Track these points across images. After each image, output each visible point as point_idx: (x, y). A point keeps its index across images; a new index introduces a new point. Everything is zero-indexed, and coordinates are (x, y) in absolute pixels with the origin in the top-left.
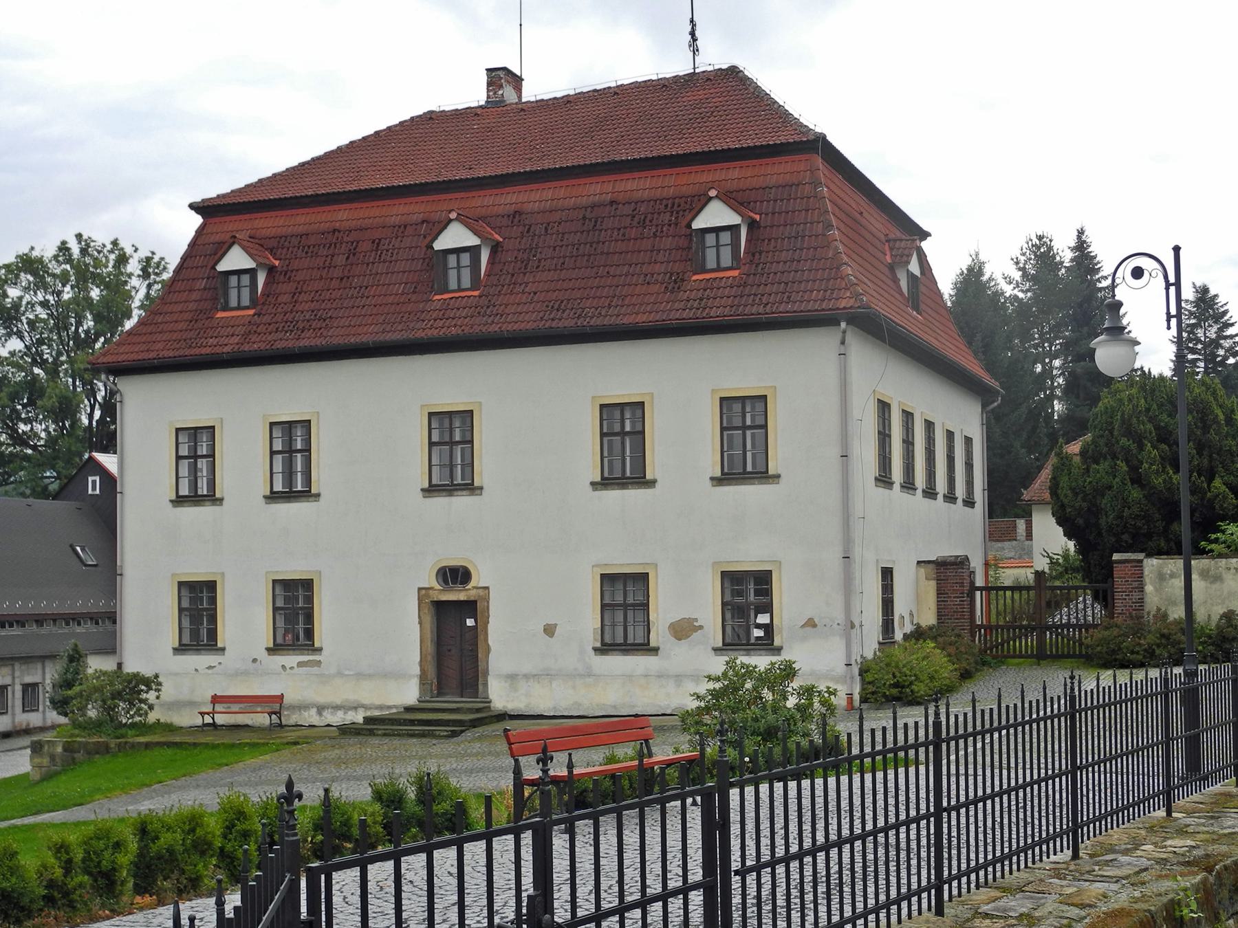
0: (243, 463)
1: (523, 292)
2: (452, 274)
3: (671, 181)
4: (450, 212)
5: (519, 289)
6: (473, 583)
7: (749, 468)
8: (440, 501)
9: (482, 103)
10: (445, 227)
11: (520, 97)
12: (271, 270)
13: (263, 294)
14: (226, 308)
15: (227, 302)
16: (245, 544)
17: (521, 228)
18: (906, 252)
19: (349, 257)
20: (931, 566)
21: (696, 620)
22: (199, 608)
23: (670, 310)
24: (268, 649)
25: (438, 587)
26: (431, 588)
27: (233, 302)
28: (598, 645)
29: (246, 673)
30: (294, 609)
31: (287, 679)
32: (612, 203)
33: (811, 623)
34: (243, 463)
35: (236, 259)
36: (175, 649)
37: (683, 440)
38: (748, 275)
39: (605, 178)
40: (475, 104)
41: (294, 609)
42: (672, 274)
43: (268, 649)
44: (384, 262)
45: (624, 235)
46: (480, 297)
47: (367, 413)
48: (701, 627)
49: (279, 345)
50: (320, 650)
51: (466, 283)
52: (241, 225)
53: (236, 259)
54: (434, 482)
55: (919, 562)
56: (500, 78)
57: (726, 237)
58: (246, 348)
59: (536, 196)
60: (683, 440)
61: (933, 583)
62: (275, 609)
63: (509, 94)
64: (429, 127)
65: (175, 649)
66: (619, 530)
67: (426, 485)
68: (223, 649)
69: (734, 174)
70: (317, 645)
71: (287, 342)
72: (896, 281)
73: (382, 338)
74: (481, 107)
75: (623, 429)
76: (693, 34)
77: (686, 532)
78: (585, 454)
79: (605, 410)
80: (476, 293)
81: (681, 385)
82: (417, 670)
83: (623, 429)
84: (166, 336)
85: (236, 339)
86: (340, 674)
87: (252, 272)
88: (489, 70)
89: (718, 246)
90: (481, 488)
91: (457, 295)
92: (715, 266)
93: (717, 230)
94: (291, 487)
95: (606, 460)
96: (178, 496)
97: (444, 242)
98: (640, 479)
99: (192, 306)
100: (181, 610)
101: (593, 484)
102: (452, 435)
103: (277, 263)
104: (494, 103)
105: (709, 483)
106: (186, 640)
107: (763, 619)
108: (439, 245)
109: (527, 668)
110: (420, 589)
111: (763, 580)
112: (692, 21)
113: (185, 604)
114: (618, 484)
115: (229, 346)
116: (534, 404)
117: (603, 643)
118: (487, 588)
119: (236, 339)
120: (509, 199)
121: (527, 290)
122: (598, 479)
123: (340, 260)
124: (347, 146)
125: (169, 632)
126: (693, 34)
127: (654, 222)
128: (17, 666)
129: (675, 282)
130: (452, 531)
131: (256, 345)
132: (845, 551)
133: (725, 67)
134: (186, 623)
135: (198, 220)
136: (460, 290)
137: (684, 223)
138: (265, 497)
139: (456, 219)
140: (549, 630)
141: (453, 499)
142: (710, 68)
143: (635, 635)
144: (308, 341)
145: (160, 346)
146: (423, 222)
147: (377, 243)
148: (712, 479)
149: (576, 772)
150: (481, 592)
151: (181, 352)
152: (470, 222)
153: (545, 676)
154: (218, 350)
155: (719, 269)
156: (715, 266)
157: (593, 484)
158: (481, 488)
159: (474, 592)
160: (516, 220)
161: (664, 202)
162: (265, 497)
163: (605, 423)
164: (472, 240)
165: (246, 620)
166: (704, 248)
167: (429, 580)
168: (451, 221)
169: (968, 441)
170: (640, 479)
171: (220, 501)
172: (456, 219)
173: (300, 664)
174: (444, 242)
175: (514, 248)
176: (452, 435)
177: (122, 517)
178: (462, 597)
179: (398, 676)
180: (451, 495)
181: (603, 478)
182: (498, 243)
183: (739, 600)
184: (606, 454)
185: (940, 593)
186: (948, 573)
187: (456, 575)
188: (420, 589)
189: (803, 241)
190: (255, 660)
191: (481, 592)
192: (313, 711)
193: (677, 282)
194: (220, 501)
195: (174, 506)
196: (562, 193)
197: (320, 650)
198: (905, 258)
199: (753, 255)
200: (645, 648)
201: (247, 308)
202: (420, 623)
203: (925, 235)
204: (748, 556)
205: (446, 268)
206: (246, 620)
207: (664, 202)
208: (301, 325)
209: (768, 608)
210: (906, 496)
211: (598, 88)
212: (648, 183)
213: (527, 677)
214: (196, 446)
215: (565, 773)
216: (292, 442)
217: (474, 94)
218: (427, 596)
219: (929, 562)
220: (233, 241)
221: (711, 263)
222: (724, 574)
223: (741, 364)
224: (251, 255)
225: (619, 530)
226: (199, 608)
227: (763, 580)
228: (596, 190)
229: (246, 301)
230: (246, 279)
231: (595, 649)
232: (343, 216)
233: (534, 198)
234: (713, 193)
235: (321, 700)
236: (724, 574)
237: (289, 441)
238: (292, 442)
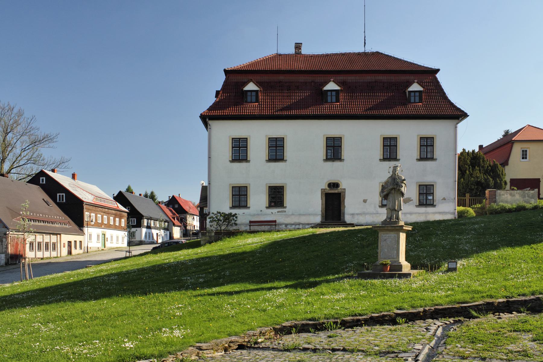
6: (340, 187)
24: (267, 207)
29: (258, 215)
30: (276, 196)
33: (444, 199)
37: (258, 149)
41: (276, 196)
50: (286, 207)
56: (298, 46)
69: (259, 78)
78: (378, 151)
82: (320, 213)
86: (293, 214)
89: (415, 96)
93: (415, 92)
97: (247, 88)
98: (245, 159)
105: (415, 161)
107: (430, 198)
109: (357, 212)
130: (332, 172)
140: (365, 201)
141: (334, 163)
143: (243, 204)
149: (108, 245)
152: (257, 83)
153: (364, 214)
166: (327, 96)
167: (325, 186)
170: (245, 159)
173: (278, 212)
174: (247, 88)
178: (336, 191)
179: (316, 215)
187: (334, 185)
188: (322, 189)
192: (284, 226)
194: (399, 160)
197: (286, 207)
200: (433, 205)
202: (322, 199)
204: (428, 180)
213: (358, 214)
215: (100, 245)
220: (251, 80)
231: (379, 206)
232: (282, 78)
235: (286, 222)
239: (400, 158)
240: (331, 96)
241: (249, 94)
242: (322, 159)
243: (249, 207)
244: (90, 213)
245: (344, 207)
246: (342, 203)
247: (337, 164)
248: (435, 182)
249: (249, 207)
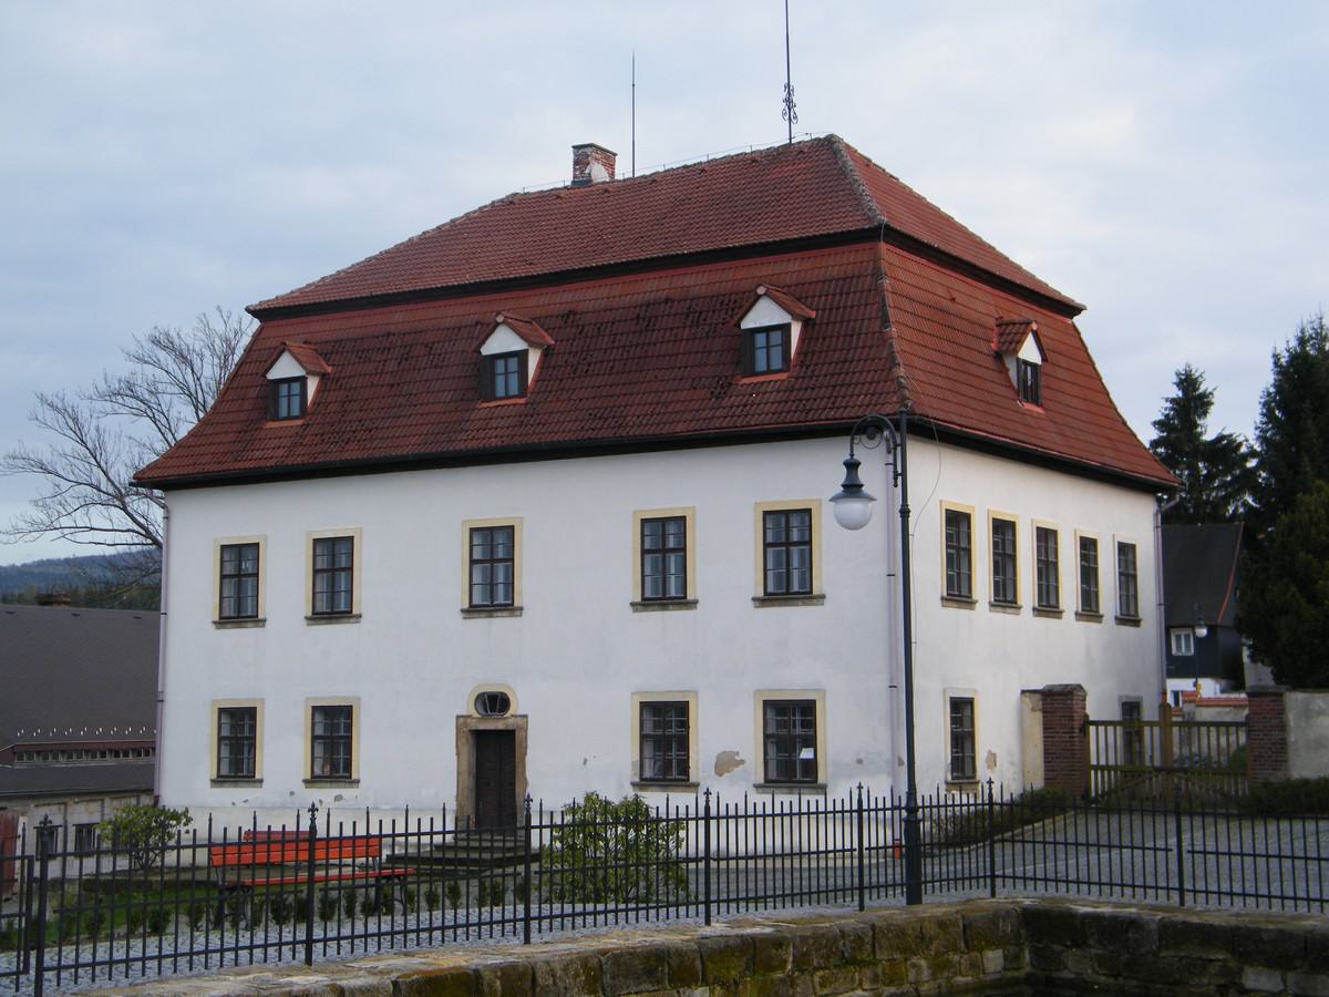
0: (286, 582)
1: (569, 400)
2: (500, 381)
3: (730, 275)
4: (498, 313)
5: (565, 395)
6: (511, 711)
7: (796, 588)
8: (480, 624)
9: (568, 183)
10: (492, 331)
11: (612, 175)
12: (323, 377)
13: (314, 403)
14: (276, 418)
15: (277, 412)
16: (285, 666)
17: (574, 330)
18: (1016, 338)
19: (377, 375)
20: (1038, 696)
21: (737, 754)
22: (238, 735)
23: (711, 419)
25: (476, 715)
26: (470, 716)
27: (283, 412)
28: (637, 780)
30: (333, 733)
31: (340, 811)
32: (667, 301)
34: (286, 582)
35: (286, 367)
36: (213, 781)
37: (726, 558)
38: (797, 378)
39: (663, 274)
40: (560, 185)
41: (333, 733)
42: (720, 378)
43: (305, 781)
44: (436, 367)
45: (676, 336)
46: (526, 404)
47: (410, 529)
48: (742, 762)
49: (321, 458)
51: (514, 390)
52: (295, 329)
53: (286, 367)
54: (475, 602)
55: (1023, 692)
56: (584, 155)
57: (776, 337)
58: (289, 461)
59: (591, 294)
60: (726, 558)
61: (1039, 715)
62: (314, 738)
63: (598, 173)
64: (517, 210)
65: (213, 781)
66: (660, 654)
67: (466, 606)
68: (261, 781)
69: (791, 268)
70: (354, 777)
71: (336, 456)
72: (1004, 371)
73: (423, 450)
74: (566, 188)
75: (664, 544)
76: (789, 101)
77: (728, 657)
79: (768, 517)
80: (522, 401)
81: (723, 498)
83: (664, 544)
84: (213, 449)
85: (281, 452)
87: (302, 380)
88: (576, 148)
90: (521, 609)
91: (503, 403)
92: (765, 369)
93: (767, 330)
94: (492, 598)
95: (770, 574)
96: (471, 605)
99: (243, 416)
100: (220, 739)
101: (633, 604)
102: (493, 554)
103: (329, 369)
104: (582, 182)
106: (225, 771)
107: (806, 754)
108: (487, 350)
110: (458, 717)
111: (806, 710)
112: (788, 86)
113: (226, 732)
114: (659, 605)
115: (273, 457)
116: (574, 521)
117: (642, 779)
118: (525, 716)
119: (281, 452)
120: (564, 298)
121: (573, 397)
122: (639, 599)
123: (392, 366)
124: (420, 237)
125: (207, 765)
126: (789, 101)
127: (708, 321)
128: (107, 801)
129: (722, 387)
131: (300, 458)
132: (891, 679)
133: (822, 136)
134: (225, 752)
135: (256, 323)
136: (507, 397)
137: (733, 322)
138: (215, 623)
139: (503, 323)
142: (807, 138)
144: (351, 454)
145: (205, 459)
146: (477, 323)
147: (429, 346)
148: (754, 599)
150: (519, 721)
151: (224, 467)
152: (786, 295)
154: (262, 464)
155: (769, 372)
156: (765, 369)
157: (633, 604)
158: (521, 609)
159: (511, 721)
160: (570, 321)
161: (721, 298)
162: (306, 618)
163: (807, 524)
164: (517, 344)
165: (284, 750)
167: (467, 707)
168: (498, 324)
169: (1126, 551)
171: (693, 604)
172: (503, 323)
175: (571, 350)
176: (493, 554)
177: (165, 639)
178: (500, 726)
180: (491, 617)
181: (644, 599)
182: (549, 346)
183: (784, 732)
184: (770, 566)
185: (1047, 727)
186: (1058, 708)
187: (495, 702)
188: (458, 717)
189: (858, 339)
190: (292, 793)
191: (519, 721)
193: (724, 387)
194: (693, 604)
195: (218, 628)
196: (617, 290)
198: (1013, 345)
199: (806, 355)
201: (297, 418)
202: (458, 754)
203: (1073, 310)
204: (792, 683)
205: (493, 375)
206: (284, 750)
207: (721, 298)
208: (346, 437)
209: (811, 742)
210: (1003, 618)
211: (689, 163)
212: (705, 278)
214: (240, 570)
216: (333, 562)
217: (557, 174)
218: (465, 724)
219: (1035, 692)
221: (761, 365)
222: (767, 704)
223: (803, 475)
224: (300, 362)
225: (660, 654)
226: (238, 735)
227: (806, 710)
228: (653, 287)
229: (296, 411)
230: (296, 387)
232: (398, 318)
233: (590, 297)
234: (761, 291)
236: (767, 704)
237: (492, 547)
238: (333, 562)
239: (825, 591)
240: (768, 347)
241: (760, 339)
242: (460, 608)
243: (358, 782)
244: (962, 848)
245: (526, 783)
246: (519, 770)
247: (501, 623)
248: (823, 692)
249: (358, 782)
